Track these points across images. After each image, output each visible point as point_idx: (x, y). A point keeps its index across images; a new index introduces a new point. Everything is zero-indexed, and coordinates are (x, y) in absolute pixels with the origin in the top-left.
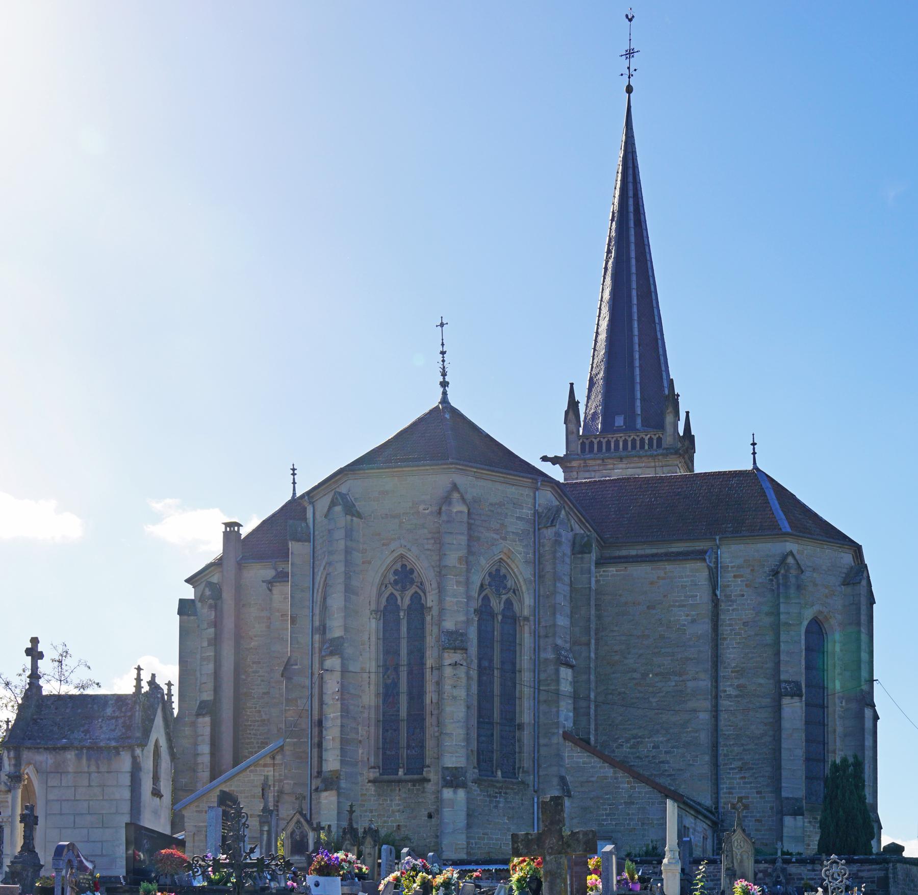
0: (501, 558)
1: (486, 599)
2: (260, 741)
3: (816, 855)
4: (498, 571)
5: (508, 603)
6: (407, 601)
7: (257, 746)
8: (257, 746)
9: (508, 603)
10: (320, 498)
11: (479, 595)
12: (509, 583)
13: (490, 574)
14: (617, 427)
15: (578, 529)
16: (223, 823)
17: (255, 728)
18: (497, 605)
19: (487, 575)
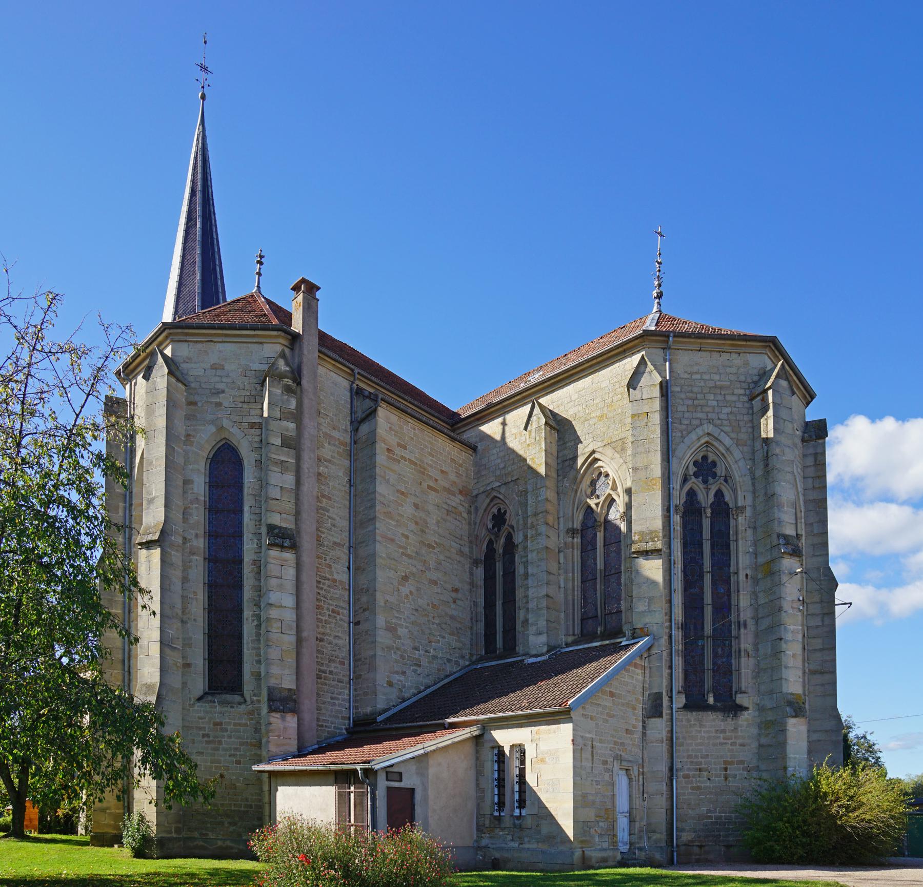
0: (707, 442)
1: (691, 494)
2: (331, 608)
3: (481, 659)
4: (705, 458)
5: (719, 494)
6: (711, 499)
7: (327, 613)
8: (327, 613)
9: (719, 494)
10: (686, 350)
11: (681, 488)
12: (720, 470)
13: (696, 463)
14: (259, 566)
15: (139, 598)
16: (319, 351)
17: (325, 587)
18: (706, 498)
19: (692, 463)
